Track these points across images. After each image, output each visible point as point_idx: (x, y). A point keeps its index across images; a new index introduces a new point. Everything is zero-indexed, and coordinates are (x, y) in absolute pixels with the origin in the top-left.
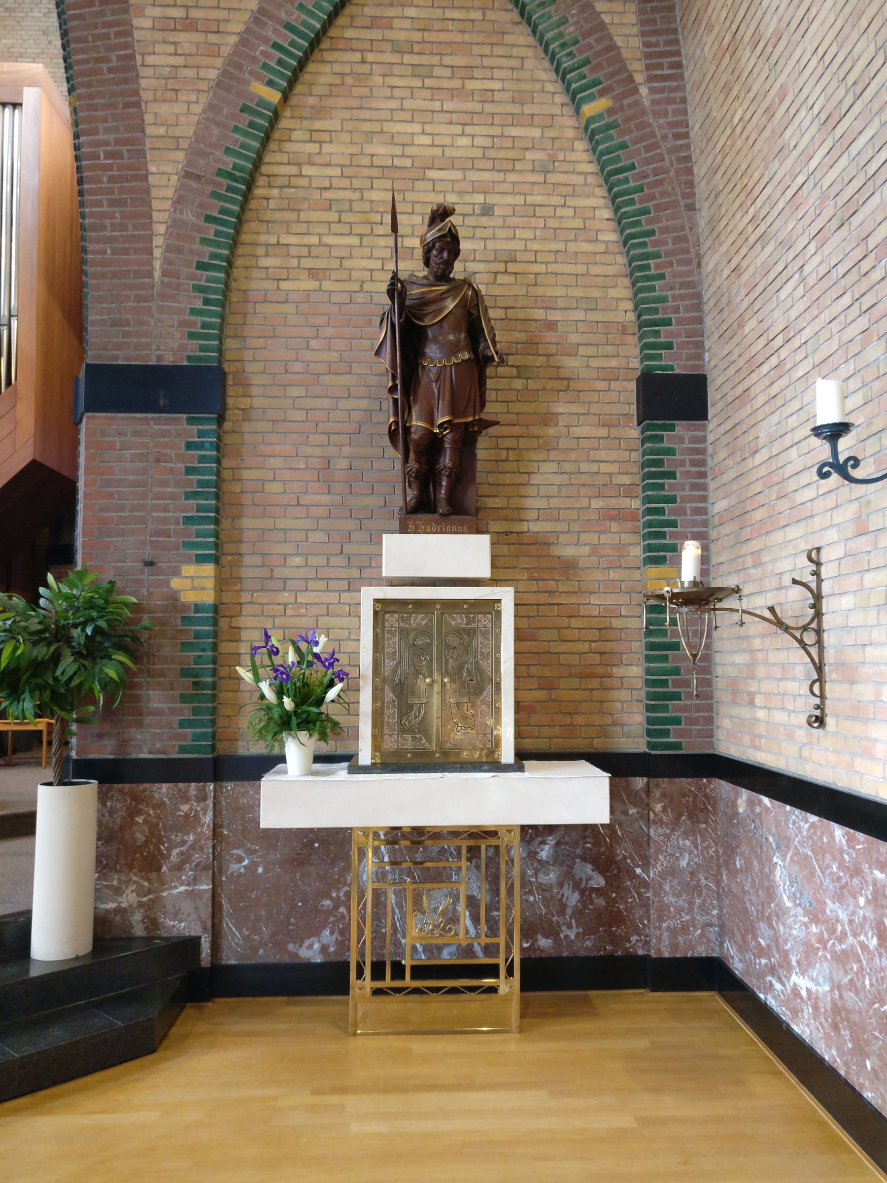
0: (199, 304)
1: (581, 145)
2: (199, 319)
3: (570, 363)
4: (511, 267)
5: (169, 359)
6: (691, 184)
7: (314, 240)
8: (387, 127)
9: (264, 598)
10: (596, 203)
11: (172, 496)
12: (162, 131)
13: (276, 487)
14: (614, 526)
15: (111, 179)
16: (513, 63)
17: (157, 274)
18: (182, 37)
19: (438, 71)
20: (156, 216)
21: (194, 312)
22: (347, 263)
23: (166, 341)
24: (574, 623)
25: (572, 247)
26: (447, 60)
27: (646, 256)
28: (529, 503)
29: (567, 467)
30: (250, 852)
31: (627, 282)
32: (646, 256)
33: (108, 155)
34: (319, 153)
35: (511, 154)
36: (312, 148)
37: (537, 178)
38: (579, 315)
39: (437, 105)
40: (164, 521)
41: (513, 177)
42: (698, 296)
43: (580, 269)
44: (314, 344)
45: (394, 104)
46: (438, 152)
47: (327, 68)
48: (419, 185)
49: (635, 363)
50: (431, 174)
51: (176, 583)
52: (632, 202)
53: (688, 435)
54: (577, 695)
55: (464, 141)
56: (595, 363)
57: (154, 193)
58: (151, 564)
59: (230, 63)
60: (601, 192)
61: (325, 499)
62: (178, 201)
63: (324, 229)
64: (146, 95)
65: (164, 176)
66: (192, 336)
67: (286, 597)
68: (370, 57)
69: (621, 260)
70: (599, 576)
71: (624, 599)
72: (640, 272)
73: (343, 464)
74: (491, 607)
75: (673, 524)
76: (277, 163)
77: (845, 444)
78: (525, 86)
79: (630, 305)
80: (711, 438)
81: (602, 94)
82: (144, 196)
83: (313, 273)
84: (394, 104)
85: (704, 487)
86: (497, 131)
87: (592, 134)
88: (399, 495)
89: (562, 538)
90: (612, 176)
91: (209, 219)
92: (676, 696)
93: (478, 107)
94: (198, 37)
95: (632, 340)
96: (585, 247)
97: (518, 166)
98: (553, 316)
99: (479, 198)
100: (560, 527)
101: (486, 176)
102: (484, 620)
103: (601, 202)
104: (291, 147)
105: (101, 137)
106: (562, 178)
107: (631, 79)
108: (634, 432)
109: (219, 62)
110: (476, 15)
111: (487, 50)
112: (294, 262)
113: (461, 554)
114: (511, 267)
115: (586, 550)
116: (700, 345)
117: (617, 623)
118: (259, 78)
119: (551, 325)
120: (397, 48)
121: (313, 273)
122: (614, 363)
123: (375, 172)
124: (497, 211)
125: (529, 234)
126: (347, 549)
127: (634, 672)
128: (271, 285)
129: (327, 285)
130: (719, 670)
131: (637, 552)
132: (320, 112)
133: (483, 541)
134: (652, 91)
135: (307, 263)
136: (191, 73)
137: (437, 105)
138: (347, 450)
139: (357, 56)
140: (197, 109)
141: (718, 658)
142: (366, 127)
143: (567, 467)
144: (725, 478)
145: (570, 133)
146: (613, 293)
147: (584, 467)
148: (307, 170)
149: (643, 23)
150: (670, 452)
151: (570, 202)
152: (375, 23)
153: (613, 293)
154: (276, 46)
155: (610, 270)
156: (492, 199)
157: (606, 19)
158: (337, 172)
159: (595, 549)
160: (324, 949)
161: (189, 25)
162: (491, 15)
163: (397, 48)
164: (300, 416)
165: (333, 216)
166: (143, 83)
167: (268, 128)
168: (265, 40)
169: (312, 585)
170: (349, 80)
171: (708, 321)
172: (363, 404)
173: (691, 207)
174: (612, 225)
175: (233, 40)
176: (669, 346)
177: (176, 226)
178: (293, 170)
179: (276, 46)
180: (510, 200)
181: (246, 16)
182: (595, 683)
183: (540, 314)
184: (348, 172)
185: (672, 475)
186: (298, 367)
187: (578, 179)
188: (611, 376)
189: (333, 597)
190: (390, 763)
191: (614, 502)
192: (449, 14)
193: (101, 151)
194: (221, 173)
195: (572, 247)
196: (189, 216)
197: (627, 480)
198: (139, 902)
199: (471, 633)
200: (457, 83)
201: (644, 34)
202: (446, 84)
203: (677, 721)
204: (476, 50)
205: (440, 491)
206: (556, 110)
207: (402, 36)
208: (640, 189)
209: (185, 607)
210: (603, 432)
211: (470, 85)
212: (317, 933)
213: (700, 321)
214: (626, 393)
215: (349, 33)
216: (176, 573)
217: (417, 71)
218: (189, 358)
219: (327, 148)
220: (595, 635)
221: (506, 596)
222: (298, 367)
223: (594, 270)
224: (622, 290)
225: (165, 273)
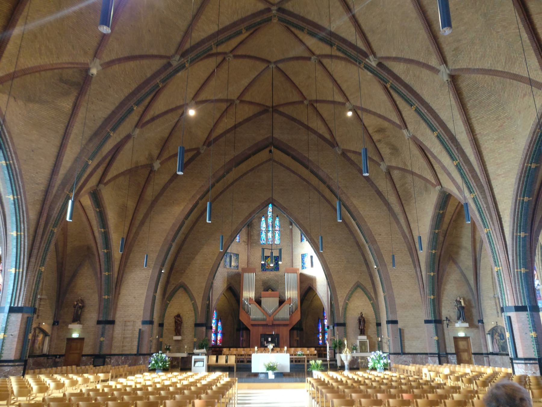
23: (342, 321)
65: (341, 308)
72: (376, 314)
76: (348, 306)
87: (372, 304)
88: (359, 333)
90: (373, 307)
113: (364, 338)
167: (347, 304)
190: (360, 352)
198: (173, 359)
205: (362, 332)
214: (375, 324)
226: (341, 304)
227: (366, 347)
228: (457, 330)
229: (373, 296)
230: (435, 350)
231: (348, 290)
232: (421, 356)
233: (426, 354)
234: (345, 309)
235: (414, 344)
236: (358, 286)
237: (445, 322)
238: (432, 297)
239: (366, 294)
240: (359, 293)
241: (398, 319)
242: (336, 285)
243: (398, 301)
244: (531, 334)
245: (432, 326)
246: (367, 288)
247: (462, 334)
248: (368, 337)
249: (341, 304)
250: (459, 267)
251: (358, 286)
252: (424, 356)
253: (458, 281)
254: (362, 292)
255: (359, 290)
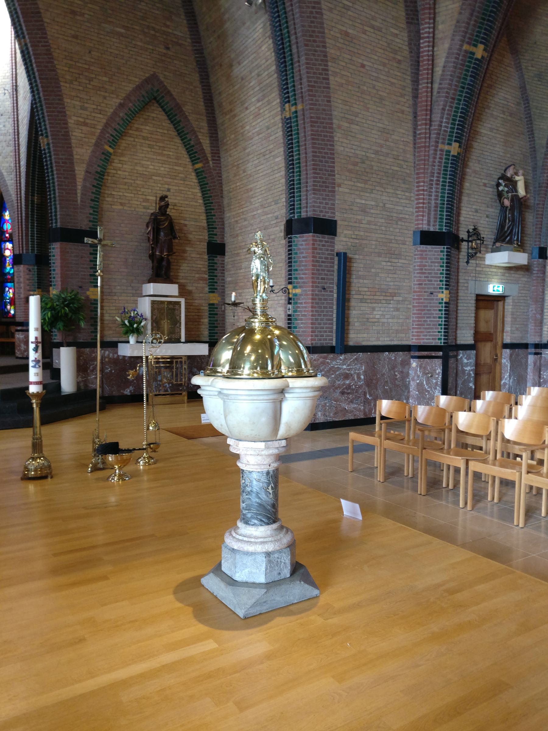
0: (91, 212)
1: (194, 174)
2: (92, 216)
3: (191, 236)
4: (175, 208)
5: (84, 228)
6: (222, 190)
7: (121, 194)
8: (141, 162)
9: (109, 298)
10: (197, 191)
11: (86, 268)
12: (79, 157)
13: (112, 266)
14: (201, 282)
15: (64, 170)
16: (176, 147)
17: (79, 201)
18: (84, 128)
19: (155, 147)
20: (78, 183)
21: (91, 214)
22: (131, 202)
24: (191, 307)
25: (191, 203)
26: (158, 144)
27: (211, 209)
28: (180, 274)
29: (190, 265)
30: (110, 367)
31: (205, 215)
32: (211, 209)
33: (63, 163)
34: (123, 168)
35: (175, 174)
36: (120, 165)
37: (182, 182)
38: (193, 223)
39: (155, 157)
40: (84, 275)
41: (176, 181)
42: (223, 222)
43: (193, 210)
44: (122, 225)
45: (143, 155)
46: (155, 171)
47: (123, 141)
48: (151, 180)
49: (207, 238)
50: (154, 177)
51: (88, 293)
52: (207, 194)
53: (220, 259)
54: (192, 326)
55: (162, 169)
56: (197, 237)
57: (77, 176)
58: (81, 287)
59: (98, 138)
60: (199, 188)
61: (126, 270)
62: (85, 180)
63: (124, 191)
64: (73, 145)
65: (80, 171)
66: (90, 221)
67: (116, 298)
68: (136, 140)
69: (203, 208)
70: (197, 295)
71: (203, 301)
72: (209, 213)
73: (131, 261)
74: (179, 303)
75: (216, 283)
77: (273, 288)
78: (179, 155)
79: (205, 221)
80: (226, 261)
81: (201, 162)
82: (74, 177)
83: (121, 204)
84: (143, 155)
85: (224, 273)
86: (171, 167)
87: (198, 173)
88: (149, 272)
89: (189, 284)
91: (94, 186)
92: (217, 327)
93: (166, 159)
94: (88, 129)
95: (206, 231)
96: (195, 204)
97: (177, 178)
98: (186, 223)
99: (167, 186)
100: (188, 281)
101: (169, 180)
102: (177, 307)
103: (198, 191)
104: (113, 164)
105: (61, 157)
106: (189, 183)
107: (207, 159)
108: (206, 257)
109: (95, 138)
110: (166, 132)
111: (168, 143)
112: (116, 200)
113: (170, 290)
114: (175, 208)
115: (194, 288)
116: (223, 235)
117: (202, 308)
118: (107, 145)
119: (185, 225)
120: (145, 138)
121: (121, 204)
122: (201, 237)
123: (138, 175)
124: (172, 191)
125: (179, 198)
126: (133, 285)
127: (206, 321)
128: (109, 206)
129: (125, 208)
130: (227, 321)
131: (207, 289)
132: (122, 155)
133: (176, 286)
134: (213, 163)
135: (119, 201)
136: (87, 140)
137: (155, 157)
138: (131, 257)
139: (132, 139)
140: (89, 151)
141: (227, 317)
142: (136, 161)
143: (190, 265)
144: (231, 273)
145: (191, 170)
146: (201, 217)
147: (194, 265)
148: (119, 172)
149: (211, 143)
150: (216, 263)
151: (191, 190)
152: (137, 130)
153: (201, 217)
154: (111, 135)
155: (201, 211)
156: (170, 187)
157: (201, 141)
158: (127, 174)
159: (197, 287)
160: (130, 391)
161: (85, 124)
162: (170, 132)
163: (145, 138)
164: (118, 246)
165: (126, 187)
166: (73, 141)
167: (107, 158)
168: (109, 133)
169: (123, 294)
170: (130, 146)
171: (226, 229)
172: (136, 244)
173: (222, 197)
174: (201, 198)
175: (99, 131)
176: (216, 235)
177: (84, 187)
178: (115, 172)
179: (111, 135)
180: (174, 188)
181: (102, 124)
182: (196, 323)
183: (182, 222)
184: (131, 174)
185: (216, 270)
186: (118, 232)
187: (192, 184)
188: (200, 241)
189: (129, 298)
191: (201, 275)
192: (158, 130)
193: (61, 161)
194: (97, 172)
195: (191, 203)
196: (88, 185)
197: (204, 270)
199: (174, 309)
200: (160, 151)
201: (211, 147)
202: (158, 151)
203: (217, 333)
204: (166, 142)
205: (162, 272)
206: (187, 163)
207: (145, 135)
208: (209, 190)
209: (91, 300)
210: (198, 256)
211: (165, 152)
212: (128, 388)
213: (223, 228)
215: (130, 132)
216: (88, 290)
217: (150, 146)
218: (90, 228)
219: (125, 166)
220: (196, 311)
221: (183, 301)
222: (118, 232)
223: (197, 210)
224: (203, 217)
225: (81, 201)
226: (83, 153)
227: (176, 322)
228: (483, 275)
229: (206, 143)
230: (434, 337)
231: (115, 102)
232: (392, 355)
233: (407, 348)
234: (99, 178)
235: (377, 314)
236: (153, 96)
237: (464, 245)
238: (455, 149)
239: (181, 134)
240: (154, 125)
241: (338, 217)
242: (61, 67)
243: (343, 146)
244: (441, 296)
245: (436, 253)
246: (187, 109)
247: (495, 288)
248: (183, 292)
249: (83, 153)
250: (519, 68)
251: (153, 96)
252: (401, 356)
253: (511, 115)
254: (167, 124)
255: (156, 113)
